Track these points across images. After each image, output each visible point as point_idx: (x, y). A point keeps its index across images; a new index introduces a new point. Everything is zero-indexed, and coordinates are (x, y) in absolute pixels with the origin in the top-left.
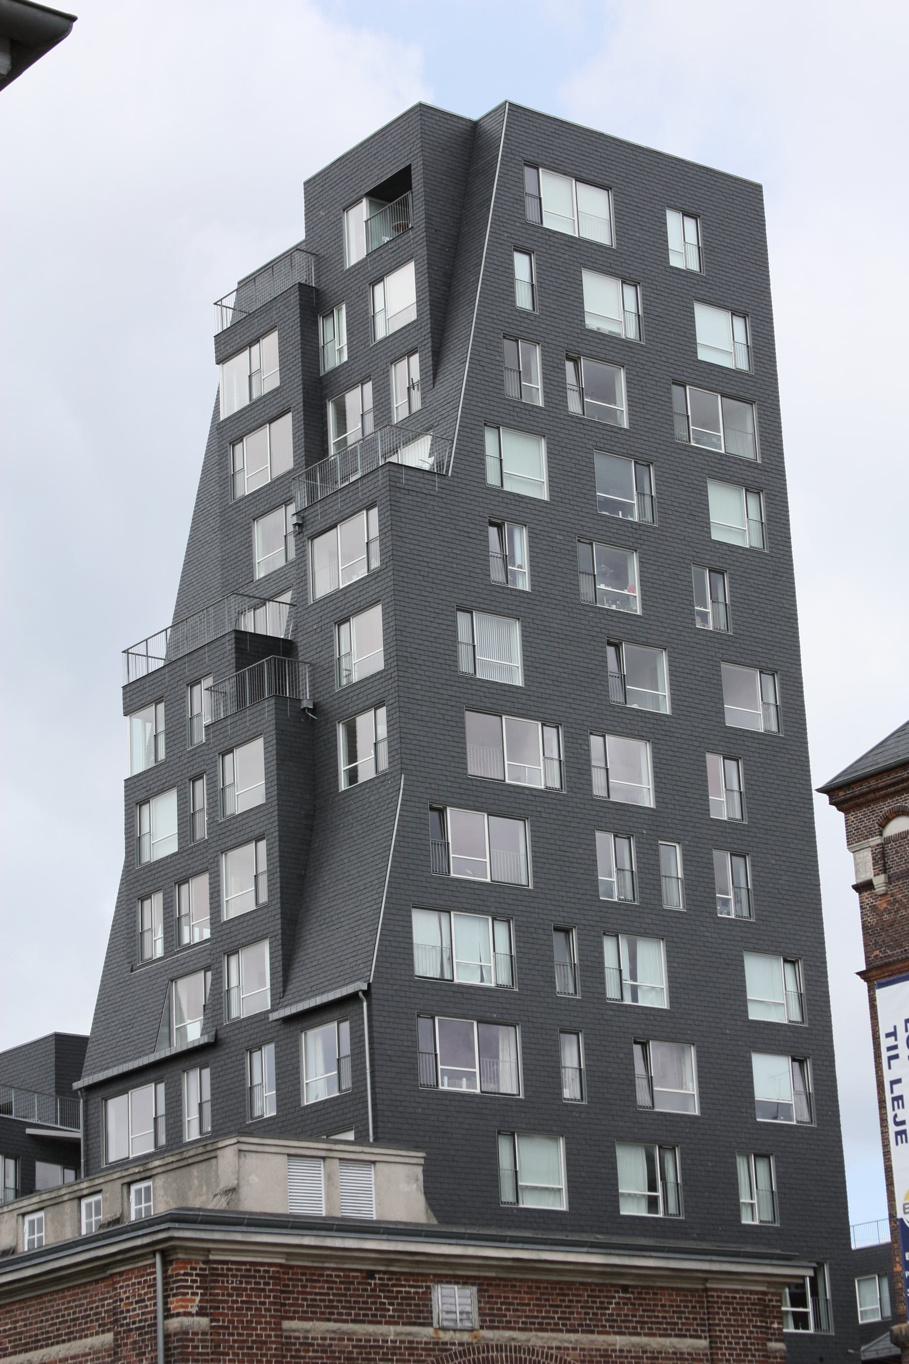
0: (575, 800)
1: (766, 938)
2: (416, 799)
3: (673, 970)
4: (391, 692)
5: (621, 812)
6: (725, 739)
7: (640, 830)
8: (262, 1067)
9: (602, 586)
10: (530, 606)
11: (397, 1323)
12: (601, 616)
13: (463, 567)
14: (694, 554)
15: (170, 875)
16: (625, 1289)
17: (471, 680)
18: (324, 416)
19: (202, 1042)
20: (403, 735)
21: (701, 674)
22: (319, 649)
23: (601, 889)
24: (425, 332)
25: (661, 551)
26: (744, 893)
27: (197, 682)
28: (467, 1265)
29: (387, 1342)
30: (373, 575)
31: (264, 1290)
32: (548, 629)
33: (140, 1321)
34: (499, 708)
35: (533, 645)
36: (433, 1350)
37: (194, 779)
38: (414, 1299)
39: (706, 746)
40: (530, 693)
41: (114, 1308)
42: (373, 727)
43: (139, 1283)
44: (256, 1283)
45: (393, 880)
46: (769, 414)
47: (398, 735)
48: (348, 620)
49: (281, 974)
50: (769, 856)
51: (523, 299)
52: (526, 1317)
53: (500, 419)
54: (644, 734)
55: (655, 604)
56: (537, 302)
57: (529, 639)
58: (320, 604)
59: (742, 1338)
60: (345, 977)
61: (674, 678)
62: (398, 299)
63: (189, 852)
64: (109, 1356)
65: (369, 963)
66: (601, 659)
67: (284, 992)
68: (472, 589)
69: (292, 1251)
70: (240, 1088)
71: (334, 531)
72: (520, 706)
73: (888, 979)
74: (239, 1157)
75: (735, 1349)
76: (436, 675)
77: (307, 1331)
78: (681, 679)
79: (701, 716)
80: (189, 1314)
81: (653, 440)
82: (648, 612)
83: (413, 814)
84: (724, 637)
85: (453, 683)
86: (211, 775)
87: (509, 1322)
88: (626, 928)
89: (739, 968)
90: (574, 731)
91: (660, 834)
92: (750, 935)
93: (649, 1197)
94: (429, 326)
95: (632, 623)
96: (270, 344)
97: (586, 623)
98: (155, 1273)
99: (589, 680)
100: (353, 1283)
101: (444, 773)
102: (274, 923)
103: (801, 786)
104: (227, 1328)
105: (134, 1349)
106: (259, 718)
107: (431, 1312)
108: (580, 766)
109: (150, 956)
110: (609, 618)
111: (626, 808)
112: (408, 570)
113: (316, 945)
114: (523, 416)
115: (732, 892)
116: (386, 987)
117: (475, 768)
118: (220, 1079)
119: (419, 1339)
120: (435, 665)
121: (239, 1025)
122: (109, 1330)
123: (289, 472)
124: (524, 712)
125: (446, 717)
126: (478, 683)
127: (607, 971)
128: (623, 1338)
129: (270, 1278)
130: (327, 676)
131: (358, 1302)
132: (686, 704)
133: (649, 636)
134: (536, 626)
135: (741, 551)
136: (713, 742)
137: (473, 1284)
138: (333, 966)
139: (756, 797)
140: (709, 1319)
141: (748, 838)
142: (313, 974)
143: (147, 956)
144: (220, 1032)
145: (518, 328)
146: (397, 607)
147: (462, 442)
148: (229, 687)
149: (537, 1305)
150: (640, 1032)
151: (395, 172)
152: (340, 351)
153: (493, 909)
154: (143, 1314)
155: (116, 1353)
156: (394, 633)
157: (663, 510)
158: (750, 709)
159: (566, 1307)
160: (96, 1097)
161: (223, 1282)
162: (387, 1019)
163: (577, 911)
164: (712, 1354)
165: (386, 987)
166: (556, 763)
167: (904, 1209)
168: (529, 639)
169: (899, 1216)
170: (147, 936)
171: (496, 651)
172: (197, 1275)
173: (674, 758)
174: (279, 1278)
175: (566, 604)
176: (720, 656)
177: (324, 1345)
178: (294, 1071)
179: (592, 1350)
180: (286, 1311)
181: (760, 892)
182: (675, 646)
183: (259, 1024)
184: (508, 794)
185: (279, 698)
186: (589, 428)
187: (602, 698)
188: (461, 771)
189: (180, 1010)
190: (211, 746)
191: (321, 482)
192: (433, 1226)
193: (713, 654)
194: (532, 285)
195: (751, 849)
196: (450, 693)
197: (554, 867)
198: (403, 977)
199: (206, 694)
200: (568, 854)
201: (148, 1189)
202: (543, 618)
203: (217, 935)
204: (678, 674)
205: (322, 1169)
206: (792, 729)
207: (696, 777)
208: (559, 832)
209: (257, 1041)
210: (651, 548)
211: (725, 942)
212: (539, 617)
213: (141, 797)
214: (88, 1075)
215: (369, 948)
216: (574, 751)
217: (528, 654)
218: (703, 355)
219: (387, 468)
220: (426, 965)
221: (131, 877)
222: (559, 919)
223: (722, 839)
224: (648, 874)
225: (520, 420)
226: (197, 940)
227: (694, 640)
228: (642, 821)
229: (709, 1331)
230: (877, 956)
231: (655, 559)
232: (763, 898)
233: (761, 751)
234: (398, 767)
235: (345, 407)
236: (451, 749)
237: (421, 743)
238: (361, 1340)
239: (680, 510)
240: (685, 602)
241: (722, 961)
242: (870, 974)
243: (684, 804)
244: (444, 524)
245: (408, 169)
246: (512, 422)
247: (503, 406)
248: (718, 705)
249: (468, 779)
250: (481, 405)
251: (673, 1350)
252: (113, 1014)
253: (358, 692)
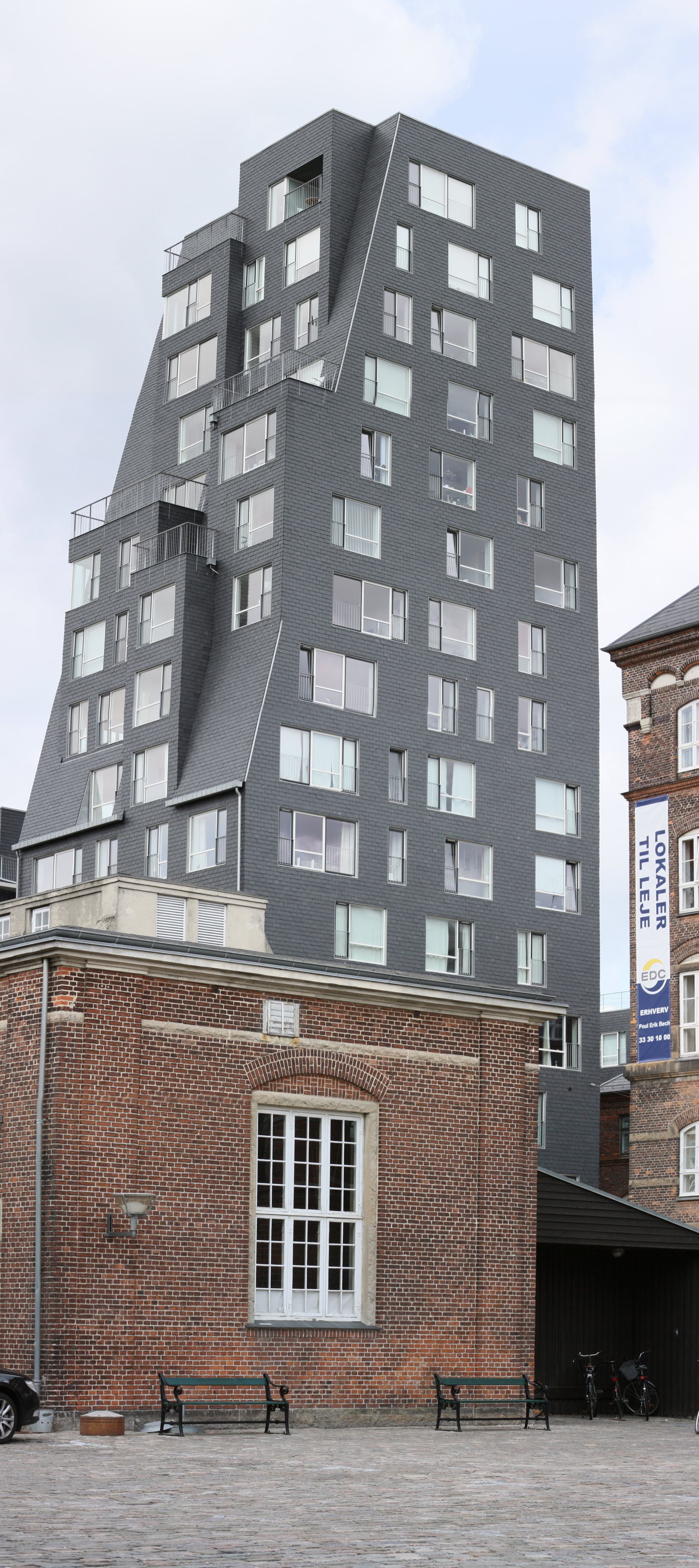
5: (449, 662)
8: (158, 841)
9: (447, 487)
11: (234, 1028)
16: (417, 1014)
17: (340, 551)
18: (242, 341)
19: (113, 820)
20: (284, 590)
21: (518, 560)
23: (429, 722)
26: (540, 732)
27: (128, 539)
28: (293, 987)
30: (269, 465)
31: (128, 995)
33: (29, 1012)
36: (261, 1050)
37: (120, 615)
38: (248, 1010)
41: (9, 1001)
42: (261, 582)
43: (30, 983)
48: (248, 499)
51: (402, 261)
52: (337, 1030)
59: (506, 1058)
62: (306, 255)
67: (178, 785)
70: (140, 857)
71: (241, 429)
72: (376, 574)
73: (645, 800)
74: (119, 893)
80: (68, 1009)
87: (323, 1033)
88: (446, 753)
92: (541, 765)
93: (449, 959)
96: (206, 283)
98: (42, 975)
104: (98, 1022)
105: (23, 1034)
107: (262, 1021)
113: (205, 749)
115: (530, 731)
117: (337, 620)
118: (125, 849)
121: (142, 808)
123: (212, 382)
125: (319, 579)
128: (412, 1051)
129: (134, 985)
131: (204, 1010)
137: (296, 1002)
140: (481, 1042)
144: (127, 813)
145: (398, 283)
148: (152, 545)
149: (347, 1022)
150: (451, 834)
151: (310, 160)
152: (259, 292)
153: (343, 731)
154: (31, 1007)
155: (8, 1036)
159: (369, 1025)
160: (29, 858)
162: (256, 811)
163: (409, 737)
164: (481, 1069)
166: (402, 621)
169: (638, 982)
170: (74, 735)
171: (362, 532)
172: (76, 979)
174: (141, 986)
179: (387, 1059)
181: (552, 733)
185: (190, 553)
191: (236, 390)
192: (270, 955)
196: (323, 560)
199: (133, 549)
201: (46, 914)
209: (156, 821)
213: (78, 626)
214: (24, 840)
218: (537, 315)
220: (289, 771)
224: (467, 712)
226: (113, 741)
229: (481, 1051)
234: (279, 614)
238: (204, 1039)
245: (320, 158)
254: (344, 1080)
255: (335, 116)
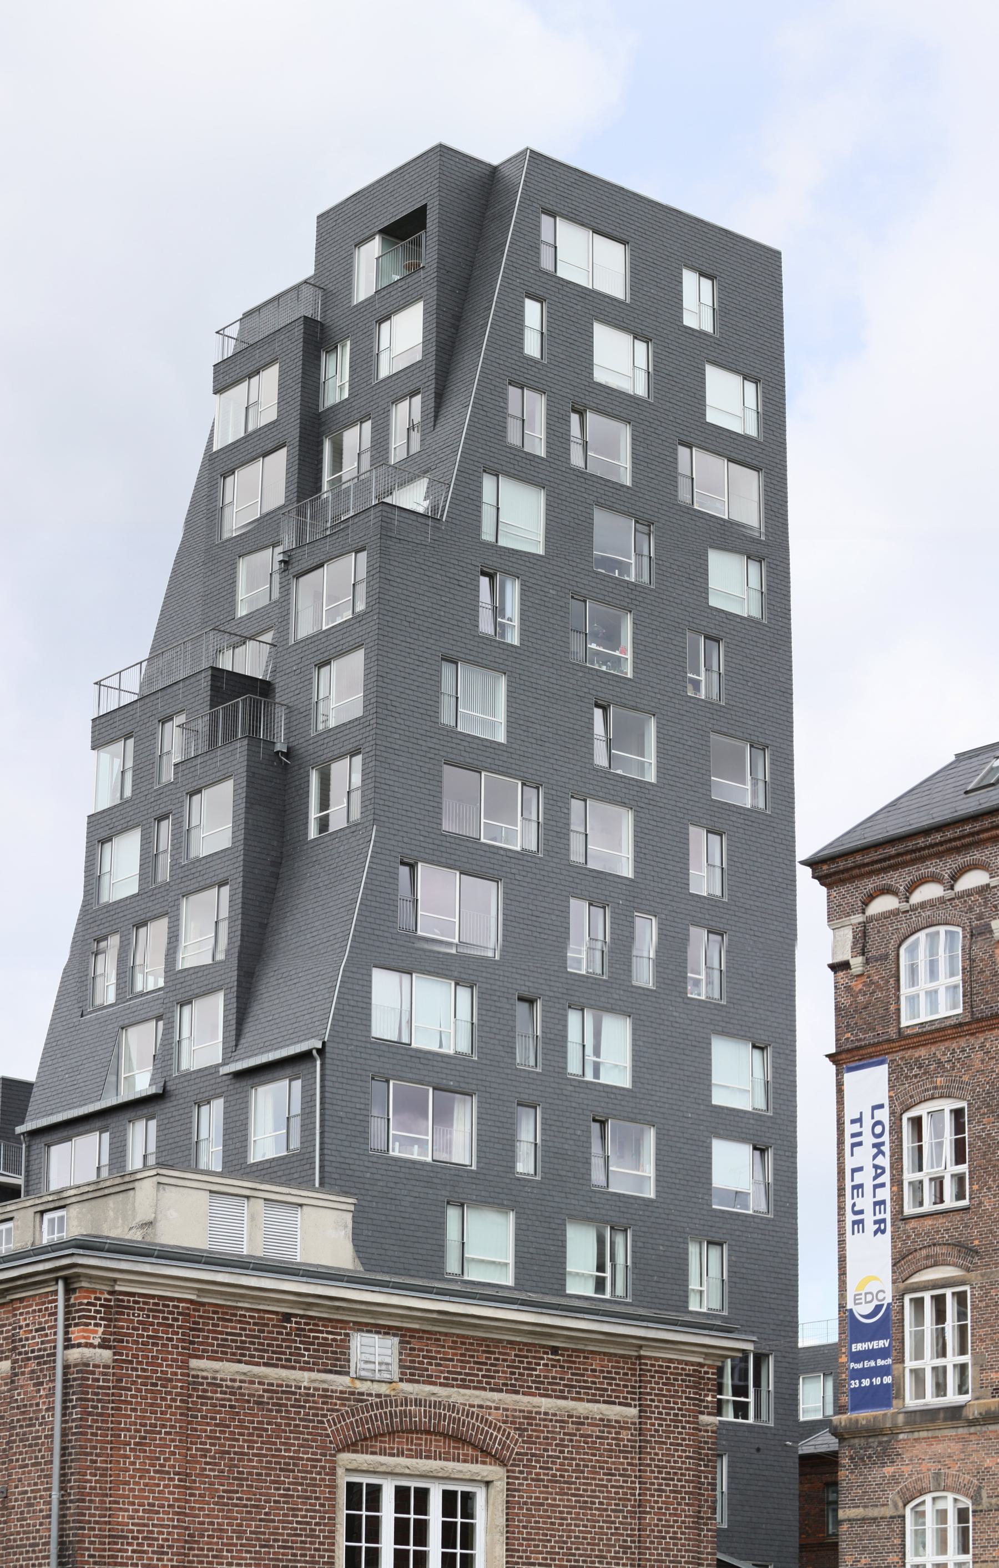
0: (551, 864)
1: (736, 1022)
2: (388, 852)
3: (637, 1048)
4: (368, 739)
6: (710, 812)
7: (616, 900)
9: (594, 646)
10: (518, 661)
12: (590, 677)
13: (451, 616)
14: (691, 619)
15: (129, 917)
16: (555, 1350)
18: (320, 452)
19: (149, 1093)
21: (689, 743)
22: (297, 692)
24: (430, 373)
25: (657, 614)
26: (716, 974)
27: (170, 718)
28: (390, 1314)
29: (300, 1388)
30: (358, 618)
31: (171, 1326)
32: (534, 686)
33: (40, 1350)
34: (479, 763)
35: (518, 701)
36: (348, 1399)
37: (160, 819)
38: (331, 1346)
39: (690, 818)
40: (512, 750)
42: (348, 775)
43: (40, 1310)
44: (164, 1318)
45: (358, 934)
46: (775, 483)
47: (373, 785)
49: (234, 1027)
50: (747, 936)
51: (532, 346)
52: (449, 1372)
53: (500, 467)
54: (627, 801)
55: (647, 668)
56: (545, 351)
57: (514, 695)
58: (301, 645)
59: (673, 1409)
60: (299, 1034)
61: (662, 746)
62: (405, 338)
63: (150, 894)
64: (6, 1384)
65: (325, 1021)
66: (587, 720)
67: (236, 1046)
68: (459, 639)
69: (204, 1287)
70: (186, 1142)
71: (320, 571)
74: (158, 1190)
75: (665, 1420)
76: (416, 725)
77: (216, 1372)
78: (669, 748)
79: (686, 787)
81: (655, 500)
82: (639, 676)
83: (383, 868)
84: (715, 707)
85: (432, 735)
86: (177, 816)
87: (430, 1376)
88: (592, 1002)
89: (706, 1051)
90: (554, 792)
91: (636, 905)
93: (598, 1277)
94: (434, 367)
95: (621, 685)
96: (271, 376)
97: (575, 682)
98: (56, 1301)
99: (574, 742)
100: (267, 1325)
101: (418, 827)
102: (230, 975)
103: (784, 866)
104: (131, 1362)
106: (230, 759)
107: (349, 1361)
108: (558, 830)
109: (101, 1002)
110: (599, 679)
111: (603, 876)
112: (394, 615)
114: (524, 465)
115: (704, 972)
116: (341, 1046)
118: (166, 1132)
119: (334, 1388)
120: (415, 715)
122: (7, 1358)
123: (280, 508)
124: (505, 770)
125: (423, 769)
126: (459, 736)
127: (570, 1046)
128: (549, 1400)
129: (179, 1314)
130: (303, 719)
131: (272, 1345)
132: (672, 773)
133: (638, 700)
134: (522, 682)
135: (739, 620)
136: (698, 814)
137: (394, 1335)
138: (288, 1022)
139: (738, 874)
140: (640, 1387)
141: (727, 916)
142: (267, 1029)
143: (98, 1001)
144: (168, 1084)
145: (527, 376)
146: (380, 652)
147: (459, 488)
148: (202, 725)
149: (462, 1361)
152: (341, 388)
153: (456, 974)
154: (43, 1343)
155: (13, 1382)
156: (375, 679)
157: (660, 572)
158: (742, 791)
159: (492, 1365)
161: (128, 1315)
162: (340, 1080)
163: (543, 982)
164: (640, 1423)
165: (341, 1046)
167: (855, 1300)
168: (514, 695)
170: (99, 981)
171: (481, 707)
172: (101, 1305)
173: (656, 828)
174: (189, 1315)
175: (555, 662)
176: (710, 726)
177: (233, 1387)
178: (243, 1128)
179: (515, 1410)
180: (194, 1350)
181: (733, 974)
182: (664, 712)
183: (209, 1077)
184: (482, 853)
185: (252, 738)
186: (591, 483)
187: (586, 761)
188: (435, 826)
189: (129, 1059)
190: (178, 785)
191: (311, 518)
192: (359, 1272)
193: (703, 723)
194: (542, 333)
195: (729, 927)
197: (526, 932)
198: (359, 1038)
199: (177, 731)
200: (540, 920)
201: (61, 1219)
202: (530, 674)
203: (170, 984)
204: (665, 742)
205: (246, 1208)
206: (780, 807)
207: (677, 849)
208: (532, 897)
209: (206, 1094)
210: (646, 610)
211: (694, 1023)
212: (526, 673)
213: (104, 835)
215: (326, 1006)
216: (554, 813)
217: (513, 710)
219: (380, 508)
220: (383, 1026)
221: (89, 917)
222: (523, 988)
223: (700, 915)
224: (620, 949)
225: (520, 469)
227: (685, 708)
228: (619, 891)
230: (848, 1038)
231: (649, 621)
232: (735, 981)
233: (746, 827)
234: (371, 817)
235: (342, 445)
236: (426, 802)
237: (396, 795)
238: (272, 1385)
239: (678, 572)
240: (678, 668)
241: (689, 1043)
242: (839, 1057)
243: (664, 876)
244: (434, 570)
245: (423, 210)
246: (512, 471)
247: (504, 453)
248: (705, 777)
249: (442, 835)
250: (481, 450)
251: (600, 1416)
252: (61, 1060)
253: (334, 737)
254: (458, 1439)
255: (443, 155)
